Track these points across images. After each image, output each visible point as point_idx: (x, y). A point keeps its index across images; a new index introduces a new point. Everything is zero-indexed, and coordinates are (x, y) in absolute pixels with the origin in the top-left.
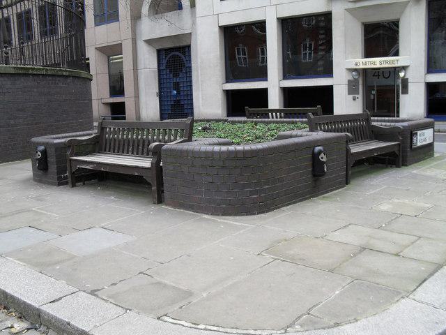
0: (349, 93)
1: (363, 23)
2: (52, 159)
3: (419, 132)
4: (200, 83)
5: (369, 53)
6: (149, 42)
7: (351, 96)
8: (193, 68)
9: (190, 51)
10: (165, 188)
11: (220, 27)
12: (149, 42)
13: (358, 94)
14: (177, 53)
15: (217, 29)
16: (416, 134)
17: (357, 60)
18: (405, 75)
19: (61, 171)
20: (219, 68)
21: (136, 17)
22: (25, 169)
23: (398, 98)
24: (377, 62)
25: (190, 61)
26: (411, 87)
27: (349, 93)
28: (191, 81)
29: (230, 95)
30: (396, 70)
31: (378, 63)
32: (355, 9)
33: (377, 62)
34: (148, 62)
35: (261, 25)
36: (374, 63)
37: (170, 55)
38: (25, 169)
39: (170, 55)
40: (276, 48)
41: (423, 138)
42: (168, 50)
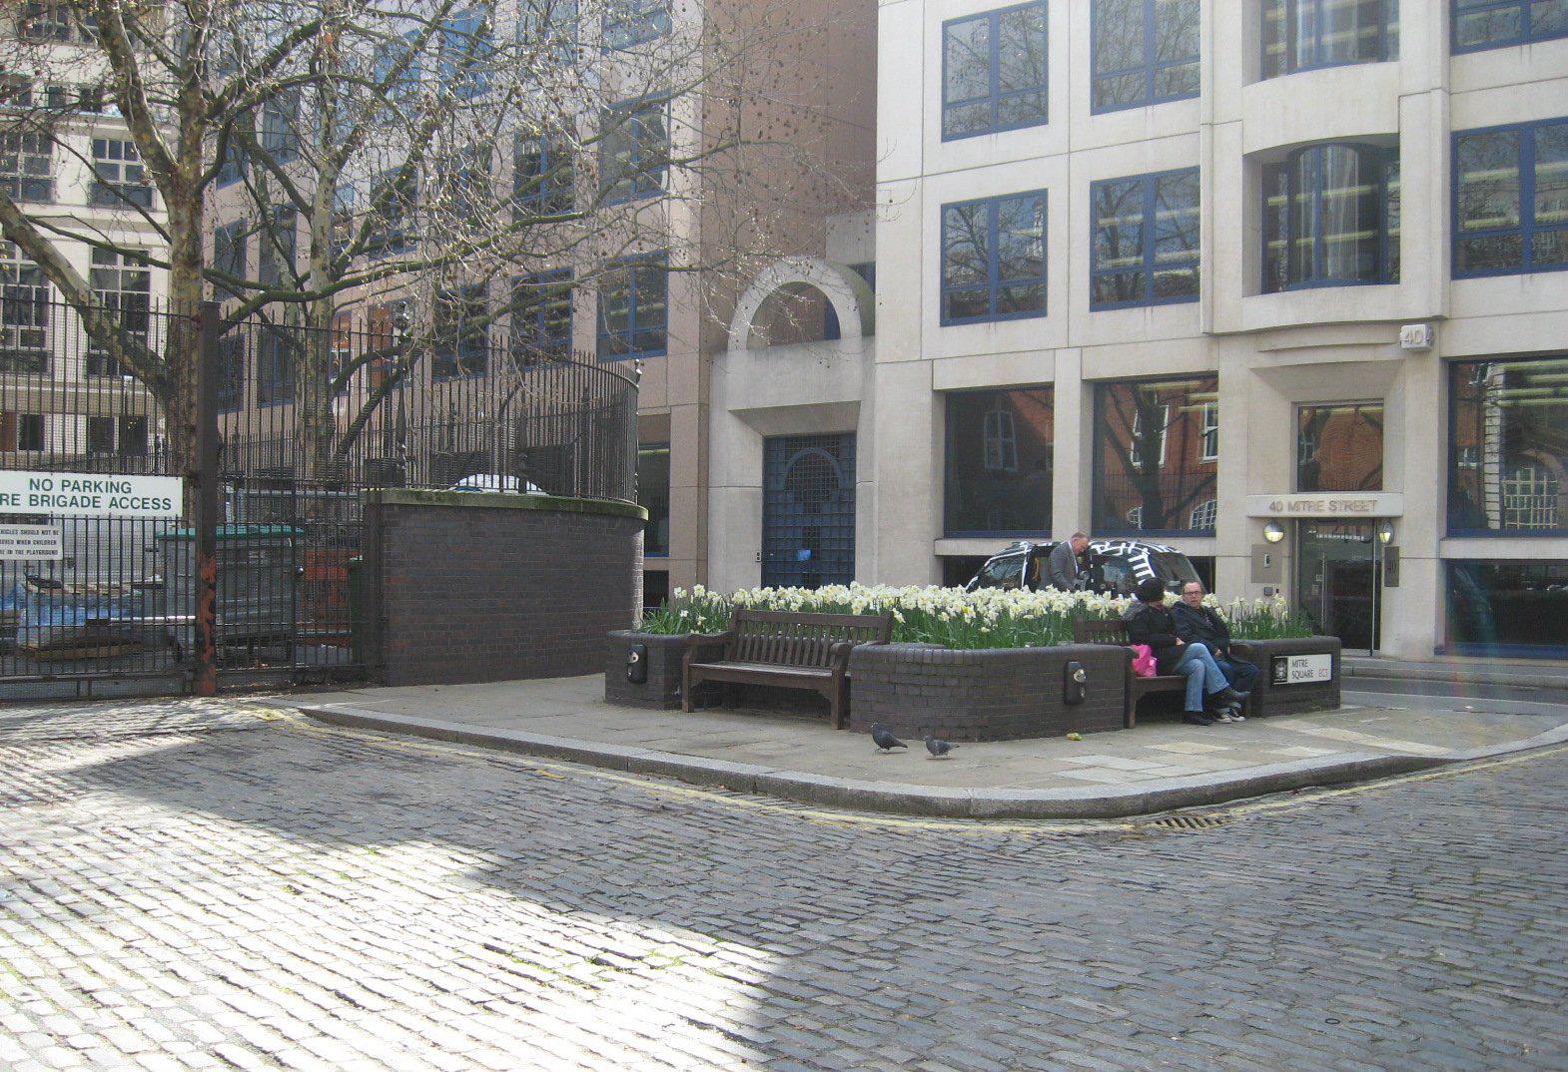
0: (1255, 579)
1: (1298, 407)
2: (657, 666)
3: (1291, 659)
4: (876, 534)
5: (1309, 479)
6: (745, 416)
7: (1261, 586)
8: (859, 495)
9: (852, 448)
10: (853, 705)
11: (937, 393)
12: (745, 416)
13: (1279, 581)
14: (814, 450)
15: (927, 399)
16: (1286, 661)
17: (1276, 498)
18: (1392, 540)
19: (674, 681)
20: (927, 498)
21: (715, 346)
22: (597, 683)
23: (1379, 593)
24: (1324, 503)
25: (852, 472)
26: (1405, 570)
27: (1255, 579)
28: (852, 528)
29: (104, 142)
30: (1376, 523)
31: (1326, 506)
32: (1273, 370)
33: (1324, 503)
34: (740, 464)
35: (1042, 394)
36: (1318, 505)
37: (796, 457)
38: (597, 683)
39: (796, 457)
40: (1077, 455)
41: (1300, 669)
42: (794, 442)
